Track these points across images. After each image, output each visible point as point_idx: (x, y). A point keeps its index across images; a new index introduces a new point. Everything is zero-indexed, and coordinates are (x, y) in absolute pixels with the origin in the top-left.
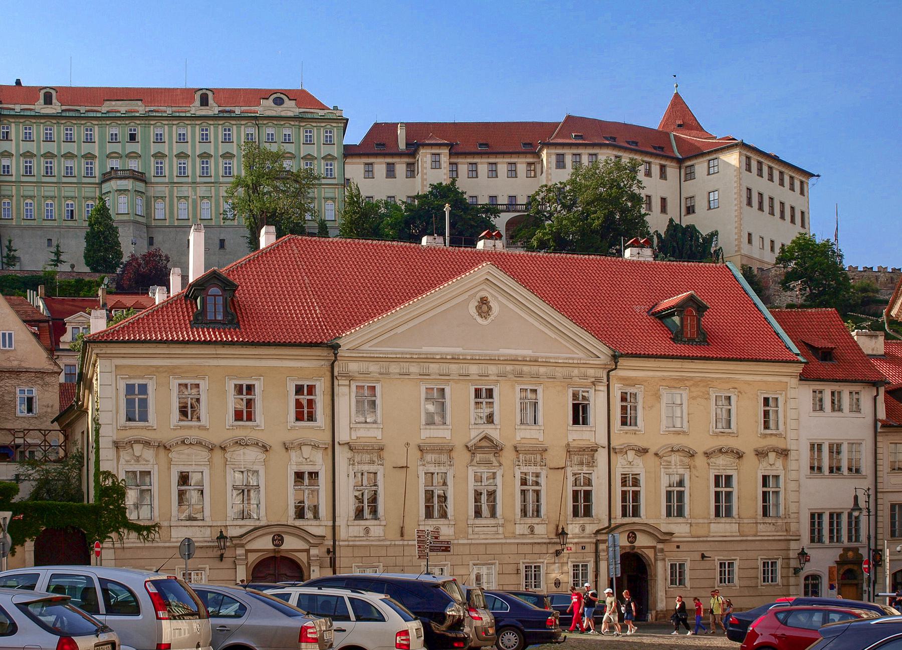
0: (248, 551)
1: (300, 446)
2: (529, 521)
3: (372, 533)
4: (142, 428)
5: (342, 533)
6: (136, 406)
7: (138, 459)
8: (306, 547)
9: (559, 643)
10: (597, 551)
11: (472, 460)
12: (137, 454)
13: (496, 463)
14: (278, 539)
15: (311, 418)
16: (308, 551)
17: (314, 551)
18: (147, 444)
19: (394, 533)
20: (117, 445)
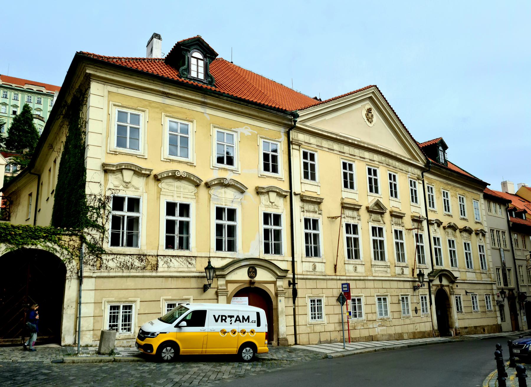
0: (228, 282)
1: (268, 192)
2: (352, 261)
3: (317, 269)
4: (132, 155)
5: (299, 269)
6: (126, 135)
7: (127, 184)
8: (273, 279)
9: (155, 383)
10: (429, 288)
11: (370, 218)
12: (127, 179)
13: (382, 222)
14: (252, 272)
15: (275, 170)
16: (274, 283)
17: (279, 283)
18: (138, 172)
19: (331, 271)
20: (106, 170)
